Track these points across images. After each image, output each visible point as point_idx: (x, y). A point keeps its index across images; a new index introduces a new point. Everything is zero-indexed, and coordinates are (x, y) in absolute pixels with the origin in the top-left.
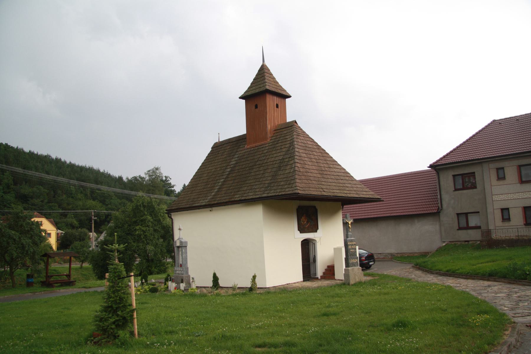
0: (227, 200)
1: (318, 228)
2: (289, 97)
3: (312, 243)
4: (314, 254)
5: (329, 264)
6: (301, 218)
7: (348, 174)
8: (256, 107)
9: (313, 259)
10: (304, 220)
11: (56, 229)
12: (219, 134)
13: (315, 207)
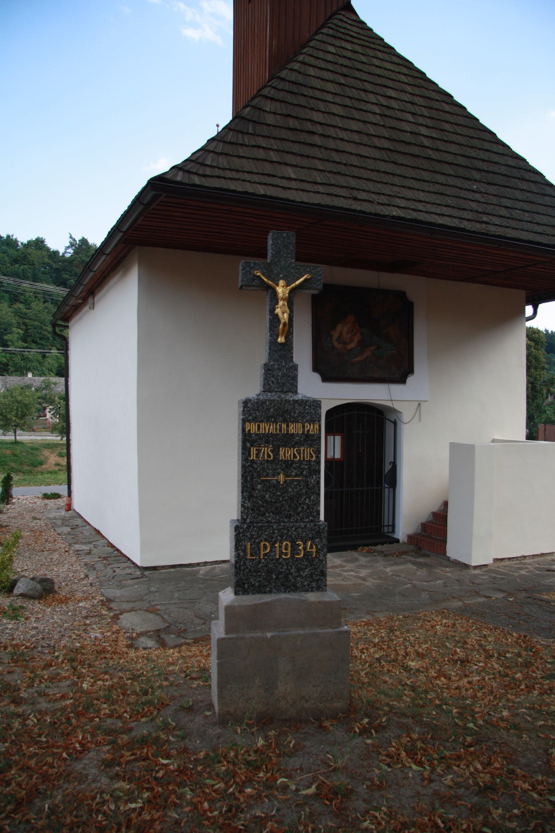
1: (411, 371)
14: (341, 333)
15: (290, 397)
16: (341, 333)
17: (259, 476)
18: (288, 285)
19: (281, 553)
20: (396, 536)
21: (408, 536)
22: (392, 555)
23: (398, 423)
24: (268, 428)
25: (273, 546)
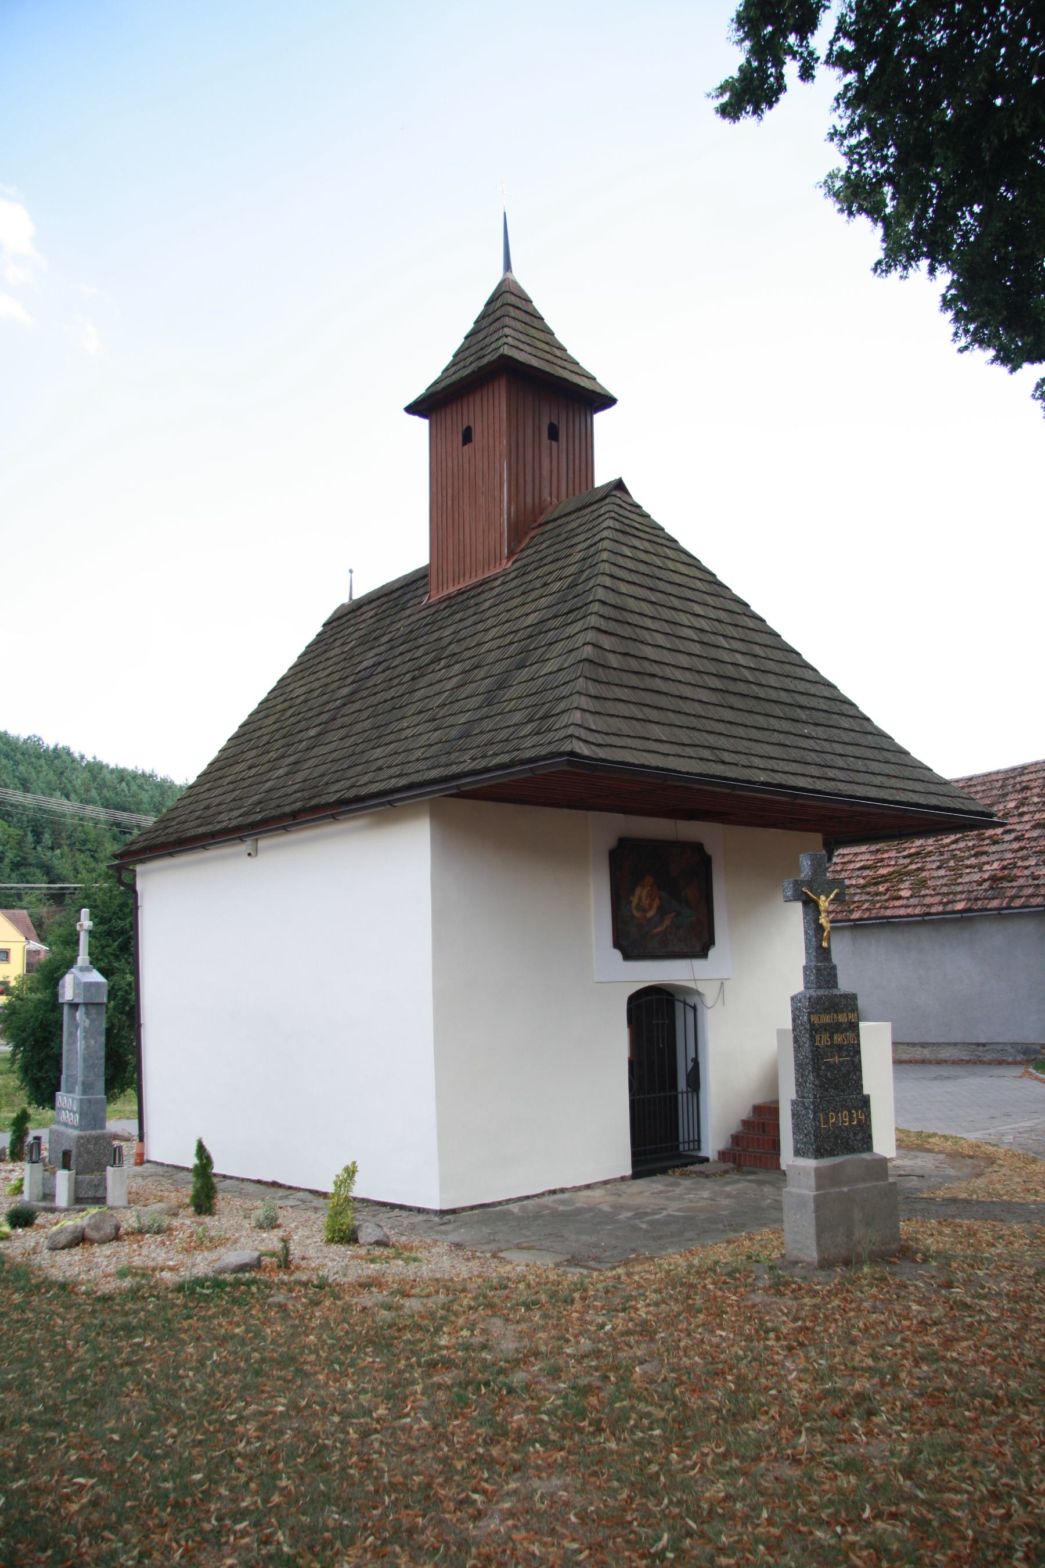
0: (298, 805)
1: (710, 942)
2: (607, 401)
3: (685, 1004)
4: (691, 1055)
5: (759, 1100)
6: (633, 893)
7: (846, 706)
8: (467, 437)
9: (688, 1076)
10: (645, 902)
11: (23, 939)
12: (351, 571)
13: (699, 847)
14: (640, 898)
15: (835, 992)
16: (640, 898)
17: (823, 1058)
18: (827, 897)
19: (843, 1121)
20: (703, 1154)
21: (719, 1153)
22: (714, 1174)
23: (699, 1008)
24: (826, 1019)
25: (837, 1116)
